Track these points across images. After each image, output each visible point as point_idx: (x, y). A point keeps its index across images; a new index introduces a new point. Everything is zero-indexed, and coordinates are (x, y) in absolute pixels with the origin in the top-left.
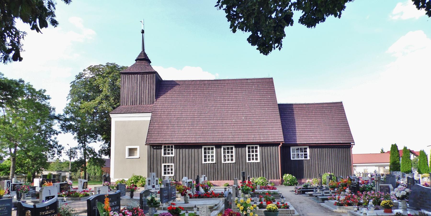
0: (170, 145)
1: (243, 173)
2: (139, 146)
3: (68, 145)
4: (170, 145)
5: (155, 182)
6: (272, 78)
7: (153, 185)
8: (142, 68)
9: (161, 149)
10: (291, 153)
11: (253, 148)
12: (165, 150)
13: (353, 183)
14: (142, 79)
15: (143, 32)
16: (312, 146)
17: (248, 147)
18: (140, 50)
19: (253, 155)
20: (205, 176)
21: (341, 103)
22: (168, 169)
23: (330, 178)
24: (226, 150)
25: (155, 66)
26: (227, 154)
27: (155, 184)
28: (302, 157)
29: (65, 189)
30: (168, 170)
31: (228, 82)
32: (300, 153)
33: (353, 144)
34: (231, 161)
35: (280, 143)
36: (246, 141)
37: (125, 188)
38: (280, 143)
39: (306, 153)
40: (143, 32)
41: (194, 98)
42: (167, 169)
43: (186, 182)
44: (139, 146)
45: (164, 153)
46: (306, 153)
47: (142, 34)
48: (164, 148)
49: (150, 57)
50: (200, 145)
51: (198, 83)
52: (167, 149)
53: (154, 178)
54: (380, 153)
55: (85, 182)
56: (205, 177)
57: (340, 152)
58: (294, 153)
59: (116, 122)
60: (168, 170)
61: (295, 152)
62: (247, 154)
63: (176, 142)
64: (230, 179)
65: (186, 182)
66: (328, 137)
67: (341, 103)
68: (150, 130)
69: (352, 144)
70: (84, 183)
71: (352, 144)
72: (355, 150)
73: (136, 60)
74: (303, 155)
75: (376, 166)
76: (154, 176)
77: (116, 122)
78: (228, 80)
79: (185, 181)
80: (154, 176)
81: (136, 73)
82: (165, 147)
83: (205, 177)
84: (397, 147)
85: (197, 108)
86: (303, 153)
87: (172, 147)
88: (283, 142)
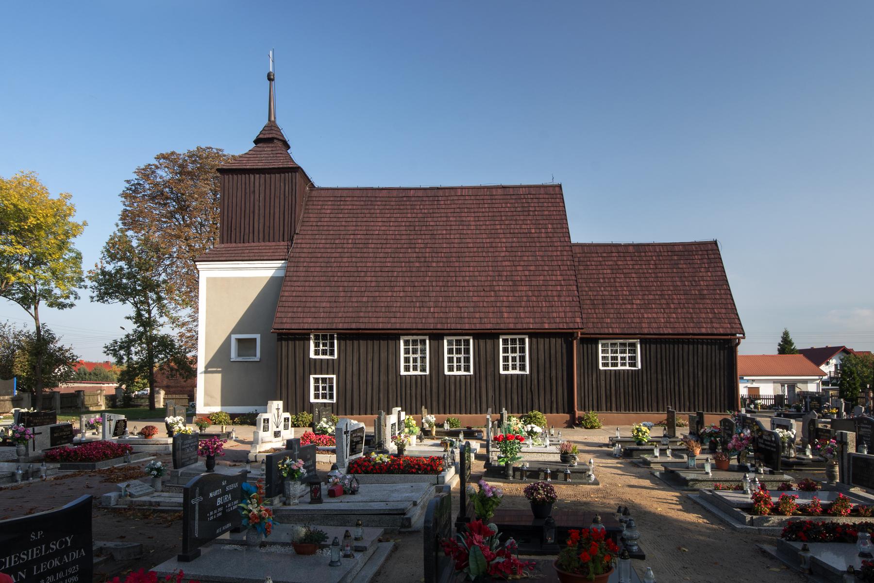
0: (328, 334)
2: (259, 335)
3: (123, 329)
4: (328, 334)
5: (283, 423)
6: (560, 186)
7: (277, 430)
8: (268, 159)
9: (309, 339)
10: (600, 355)
11: (514, 341)
13: (767, 441)
16: (650, 339)
17: (448, 341)
19: (415, 360)
20: (400, 409)
21: (715, 243)
22: (326, 390)
23: (697, 419)
24: (417, 345)
25: (299, 155)
27: (281, 427)
28: (623, 364)
29: (65, 439)
30: (326, 387)
32: (619, 355)
33: (742, 335)
35: (575, 331)
37: (196, 443)
39: (321, 398)
40: (270, 78)
41: (383, 228)
42: (327, 392)
43: (347, 432)
44: (259, 335)
45: (316, 350)
46: (321, 398)
48: (315, 339)
49: (288, 135)
50: (395, 334)
52: (321, 342)
53: (280, 414)
54: (776, 353)
55: (119, 421)
56: (399, 412)
57: (707, 365)
58: (612, 355)
59: (209, 280)
60: (326, 387)
63: (340, 326)
64: (448, 411)
65: (347, 432)
67: (715, 243)
69: (738, 335)
70: (117, 423)
71: (738, 335)
72: (743, 350)
73: (257, 141)
75: (775, 382)
76: (278, 409)
77: (209, 280)
78: (462, 188)
79: (344, 430)
80: (278, 409)
81: (253, 169)
83: (399, 412)
84: (7, 379)
85: (389, 250)
87: (332, 338)
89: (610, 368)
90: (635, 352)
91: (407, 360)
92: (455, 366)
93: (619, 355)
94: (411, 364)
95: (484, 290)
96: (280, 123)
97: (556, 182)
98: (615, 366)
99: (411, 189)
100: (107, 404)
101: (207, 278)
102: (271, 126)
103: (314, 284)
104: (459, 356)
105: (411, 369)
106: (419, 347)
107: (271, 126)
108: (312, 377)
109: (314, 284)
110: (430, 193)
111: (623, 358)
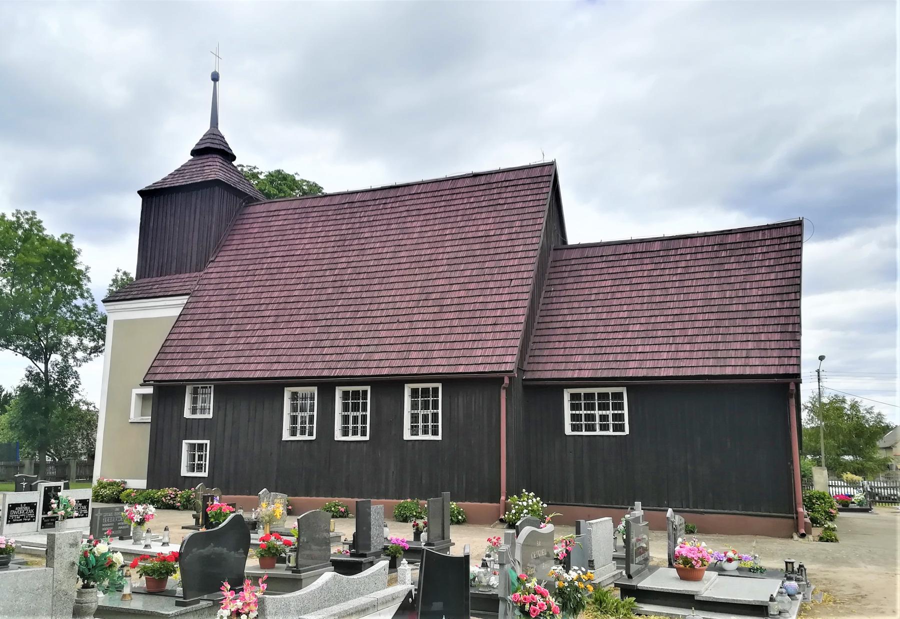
1: (183, 528)
12: (195, 400)
14: (750, 313)
15: (215, 78)
18: (206, 127)
19: (355, 419)
26: (421, 412)
28: (604, 428)
31: (764, 234)
34: (601, 430)
36: (403, 371)
38: (503, 378)
40: (215, 78)
44: (405, 438)
47: (213, 82)
51: (657, 246)
57: (195, 213)
61: (352, 403)
62: (440, 424)
66: (531, 204)
68: (168, 343)
73: (195, 153)
74: (611, 422)
82: (195, 392)
86: (610, 413)
88: (510, 374)
89: (584, 433)
90: (621, 407)
91: (414, 418)
92: (420, 427)
93: (597, 413)
94: (421, 424)
95: (398, 321)
96: (222, 129)
97: (548, 160)
98: (605, 430)
99: (357, 192)
100: (860, 476)
101: (114, 321)
102: (214, 133)
103: (695, 310)
104: (425, 412)
105: (420, 431)
106: (420, 399)
107: (214, 133)
108: (185, 443)
109: (695, 310)
110: (378, 195)
111: (604, 418)
